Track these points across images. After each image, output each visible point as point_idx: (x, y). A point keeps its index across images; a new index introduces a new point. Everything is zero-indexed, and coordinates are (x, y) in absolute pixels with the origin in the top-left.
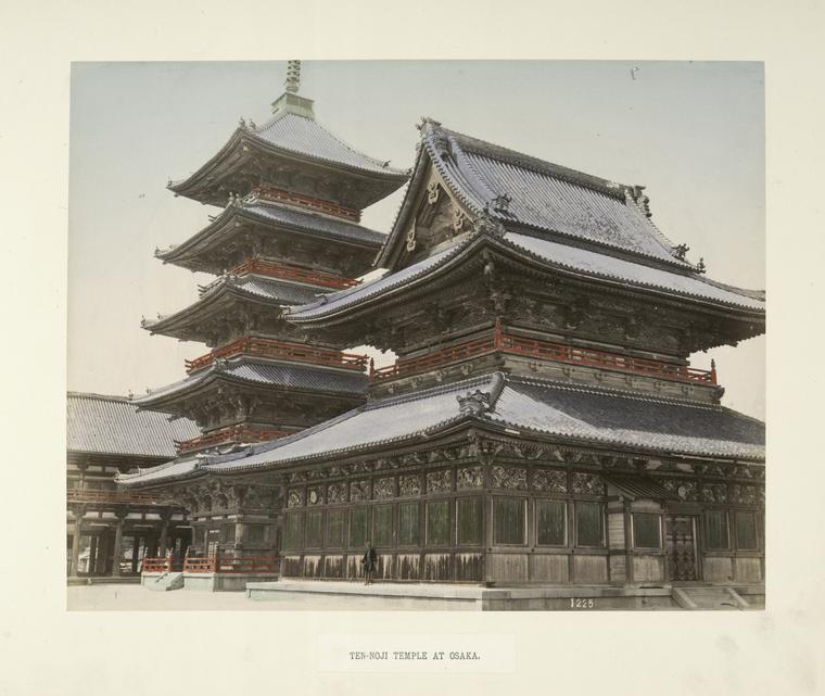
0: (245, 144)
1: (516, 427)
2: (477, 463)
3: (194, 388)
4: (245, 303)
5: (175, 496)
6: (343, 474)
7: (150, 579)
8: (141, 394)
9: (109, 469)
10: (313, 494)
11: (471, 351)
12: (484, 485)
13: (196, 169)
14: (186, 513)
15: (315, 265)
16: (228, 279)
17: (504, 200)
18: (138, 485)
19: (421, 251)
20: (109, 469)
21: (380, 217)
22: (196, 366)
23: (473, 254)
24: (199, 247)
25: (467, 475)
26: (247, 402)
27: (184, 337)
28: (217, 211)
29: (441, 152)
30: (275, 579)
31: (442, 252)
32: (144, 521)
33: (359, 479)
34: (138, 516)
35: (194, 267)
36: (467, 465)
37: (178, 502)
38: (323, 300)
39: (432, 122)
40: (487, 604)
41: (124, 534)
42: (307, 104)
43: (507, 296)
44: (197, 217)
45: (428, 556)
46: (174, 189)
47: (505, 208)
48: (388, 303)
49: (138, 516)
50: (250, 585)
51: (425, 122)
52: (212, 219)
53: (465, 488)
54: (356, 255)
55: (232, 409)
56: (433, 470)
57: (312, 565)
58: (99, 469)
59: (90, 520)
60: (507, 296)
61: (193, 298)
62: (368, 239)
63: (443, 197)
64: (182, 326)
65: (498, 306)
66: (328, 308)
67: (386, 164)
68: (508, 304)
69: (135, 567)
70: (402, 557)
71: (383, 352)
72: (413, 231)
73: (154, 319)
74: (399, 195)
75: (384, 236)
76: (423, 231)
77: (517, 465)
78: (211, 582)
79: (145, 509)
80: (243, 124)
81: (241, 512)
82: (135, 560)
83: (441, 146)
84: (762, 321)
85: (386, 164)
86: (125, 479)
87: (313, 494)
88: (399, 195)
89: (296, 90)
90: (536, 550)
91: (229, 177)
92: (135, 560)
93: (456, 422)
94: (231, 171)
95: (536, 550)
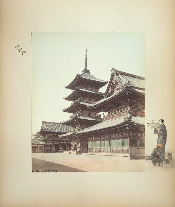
0: (78, 78)
1: (136, 124)
2: (127, 131)
3: (71, 120)
4: (79, 106)
5: (69, 139)
6: (99, 134)
7: (65, 152)
8: (62, 122)
9: (57, 135)
10: (94, 137)
11: (123, 111)
12: (129, 135)
13: (69, 84)
14: (70, 142)
15: (91, 99)
16: (76, 101)
17: (129, 82)
18: (62, 137)
19: (112, 93)
20: (57, 135)
21: (103, 90)
22: (71, 117)
23: (124, 92)
24: (71, 96)
25: (125, 133)
26: (80, 123)
27: (69, 112)
28: (73, 91)
29: (116, 74)
30: (87, 152)
31: (116, 93)
32: (63, 143)
33: (103, 135)
34: (62, 142)
35: (70, 100)
36: (125, 132)
37: (69, 140)
38: (82, 130)
39: (114, 69)
40: (131, 157)
41: (60, 145)
42: (88, 71)
43: (130, 100)
44: (71, 92)
45: (117, 149)
46: (66, 87)
47: (129, 84)
48: (107, 103)
49: (62, 142)
50: (83, 153)
51: (112, 69)
52: (72, 104)
53: (124, 136)
54: (100, 96)
55: (78, 124)
56: (117, 133)
57: (94, 150)
58: (56, 135)
59: (55, 143)
60: (130, 100)
61: (70, 105)
62: (101, 94)
63: (117, 83)
64: (68, 110)
65: (129, 102)
66: (94, 105)
67: (103, 80)
68: (130, 102)
69: (62, 150)
70: (112, 149)
71: (105, 112)
72: (110, 89)
73: (64, 109)
74: (107, 85)
75: (104, 93)
76: (112, 90)
77: (135, 132)
78: (75, 153)
79: (63, 141)
80: (78, 74)
81: (80, 141)
82: (62, 149)
83: (116, 73)
84: (144, 128)
85: (103, 80)
86: (60, 136)
87: (94, 137)
88: (107, 85)
89: (86, 68)
90: (139, 148)
91: (75, 84)
92: (62, 149)
93: (124, 123)
94: (75, 83)
95: (139, 148)
